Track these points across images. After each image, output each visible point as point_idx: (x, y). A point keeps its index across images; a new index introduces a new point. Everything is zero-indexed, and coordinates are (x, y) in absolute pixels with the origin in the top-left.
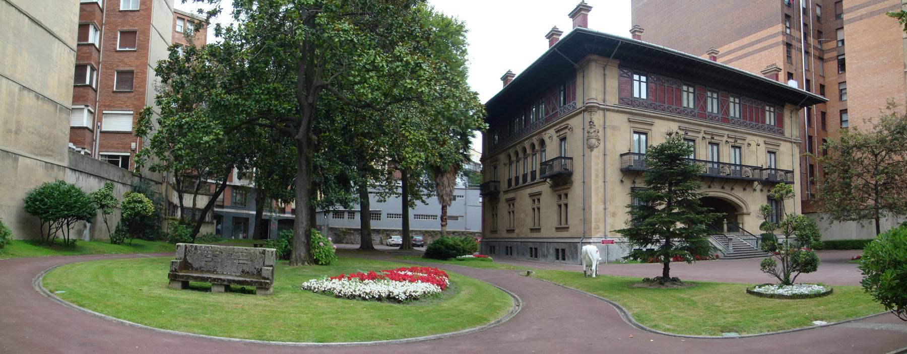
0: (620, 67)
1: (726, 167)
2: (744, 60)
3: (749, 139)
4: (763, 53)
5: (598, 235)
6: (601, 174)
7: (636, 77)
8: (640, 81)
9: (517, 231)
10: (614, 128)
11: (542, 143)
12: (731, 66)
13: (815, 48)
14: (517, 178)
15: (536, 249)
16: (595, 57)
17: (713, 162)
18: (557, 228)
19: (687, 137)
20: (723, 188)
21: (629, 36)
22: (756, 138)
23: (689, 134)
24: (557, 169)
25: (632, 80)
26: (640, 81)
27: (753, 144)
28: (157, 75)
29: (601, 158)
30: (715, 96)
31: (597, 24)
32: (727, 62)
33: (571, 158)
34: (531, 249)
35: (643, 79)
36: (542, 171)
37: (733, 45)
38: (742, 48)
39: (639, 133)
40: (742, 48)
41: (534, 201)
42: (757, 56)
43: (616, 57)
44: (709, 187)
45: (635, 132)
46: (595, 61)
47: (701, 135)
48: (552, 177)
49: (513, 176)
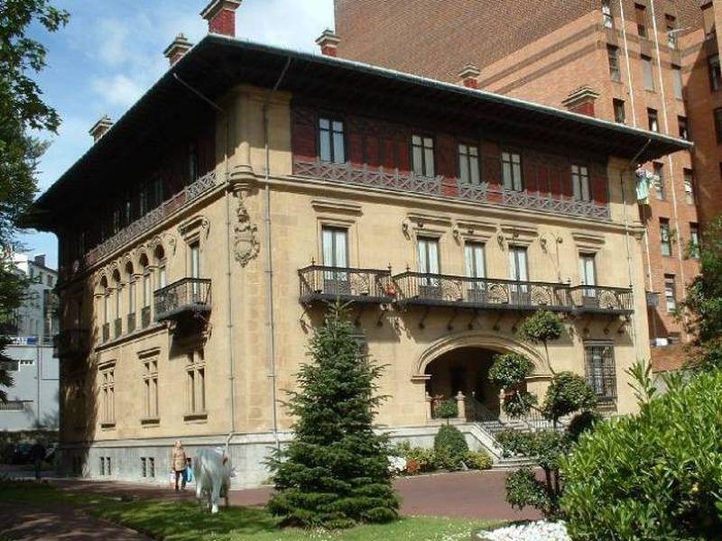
0: (292, 105)
1: (500, 287)
2: (534, 84)
3: (545, 231)
4: (566, 68)
5: (259, 429)
6: (262, 308)
7: (324, 123)
8: (331, 131)
9: (118, 427)
10: (285, 220)
11: (160, 252)
12: (515, 97)
13: (664, 49)
14: (118, 323)
15: (152, 459)
16: (244, 88)
17: (475, 279)
18: (187, 418)
19: (423, 233)
20: (496, 328)
21: (316, 51)
22: (554, 228)
23: (425, 226)
24: (186, 301)
25: (456, 156)
26: (331, 131)
27: (551, 246)
28: (13, 364)
29: (262, 279)
30: (584, 171)
31: (252, 28)
32: (506, 90)
33: (208, 281)
34: (144, 459)
35: (338, 126)
36: (160, 307)
37: (511, 60)
38: (527, 63)
39: (334, 229)
40: (527, 63)
41: (147, 365)
42: (555, 74)
43: (281, 88)
44: (470, 327)
45: (325, 227)
46: (248, 95)
47: (494, 235)
48: (172, 318)
49: (111, 320)
